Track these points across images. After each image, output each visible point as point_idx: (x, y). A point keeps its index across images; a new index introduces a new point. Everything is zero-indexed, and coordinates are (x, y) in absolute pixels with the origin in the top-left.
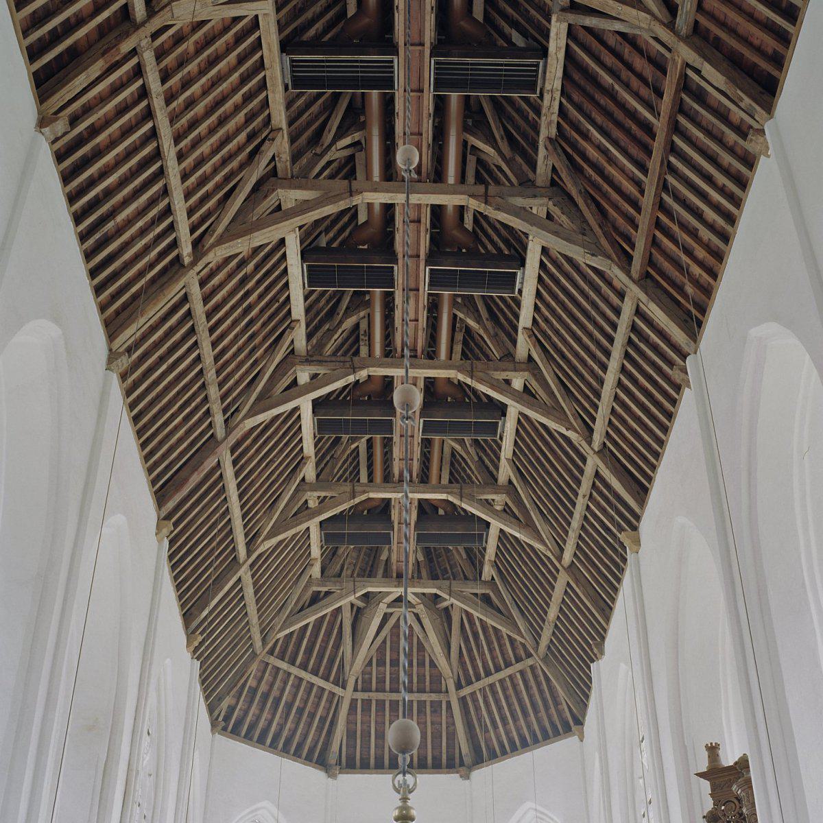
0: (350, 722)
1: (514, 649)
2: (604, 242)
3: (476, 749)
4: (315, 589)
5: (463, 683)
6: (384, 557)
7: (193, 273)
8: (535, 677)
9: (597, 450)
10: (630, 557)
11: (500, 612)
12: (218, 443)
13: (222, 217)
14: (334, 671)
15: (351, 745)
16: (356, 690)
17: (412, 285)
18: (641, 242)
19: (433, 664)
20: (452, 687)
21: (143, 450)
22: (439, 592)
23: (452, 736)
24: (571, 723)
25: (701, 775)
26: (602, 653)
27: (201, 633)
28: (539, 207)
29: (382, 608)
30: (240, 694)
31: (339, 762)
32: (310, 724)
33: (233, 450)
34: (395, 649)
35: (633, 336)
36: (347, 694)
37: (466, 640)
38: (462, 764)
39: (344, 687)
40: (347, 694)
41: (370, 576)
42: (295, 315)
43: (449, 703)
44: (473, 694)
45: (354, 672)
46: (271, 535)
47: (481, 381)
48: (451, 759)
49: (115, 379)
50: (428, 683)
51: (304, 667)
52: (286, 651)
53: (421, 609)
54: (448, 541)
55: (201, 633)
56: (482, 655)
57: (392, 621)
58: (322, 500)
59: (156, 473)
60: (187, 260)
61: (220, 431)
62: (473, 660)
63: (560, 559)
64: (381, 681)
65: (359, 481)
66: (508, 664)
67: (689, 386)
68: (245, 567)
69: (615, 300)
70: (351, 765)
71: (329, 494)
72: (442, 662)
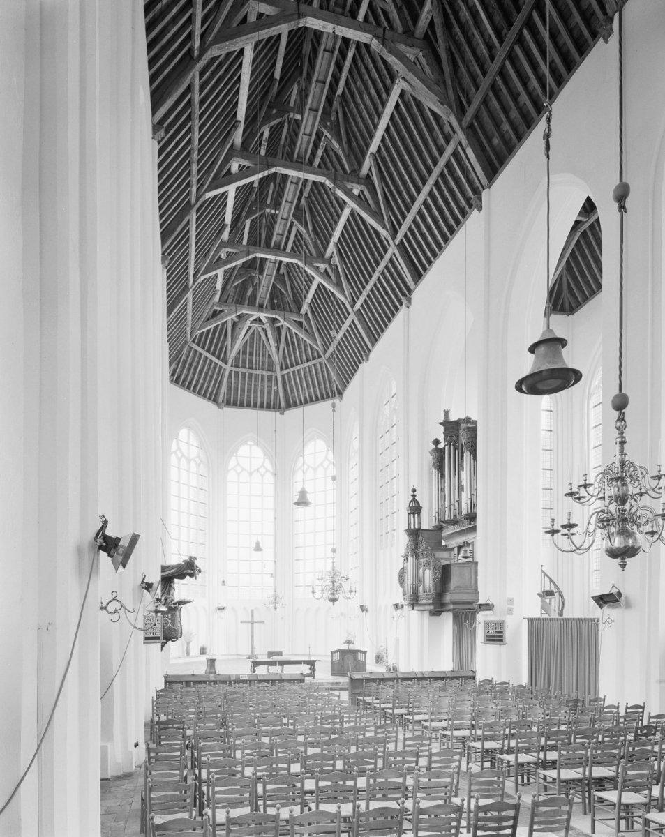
0: (229, 382)
1: (312, 353)
2: (451, 94)
3: (287, 401)
4: (215, 308)
5: (284, 368)
9: (397, 244)
11: (306, 331)
13: (218, 17)
14: (222, 354)
16: (232, 366)
17: (314, 107)
18: (477, 100)
19: (269, 356)
20: (278, 368)
22: (277, 317)
24: (336, 393)
25: (440, 423)
26: (368, 359)
28: (411, 53)
29: (248, 323)
30: (179, 362)
37: (288, 345)
38: (280, 407)
39: (226, 363)
40: (228, 368)
41: (240, 304)
43: (276, 377)
44: (288, 374)
45: (232, 356)
50: (266, 366)
52: (200, 341)
53: (267, 326)
56: (295, 354)
57: (251, 331)
62: (290, 356)
64: (244, 362)
66: (308, 360)
67: (480, 209)
69: (442, 140)
72: (274, 356)
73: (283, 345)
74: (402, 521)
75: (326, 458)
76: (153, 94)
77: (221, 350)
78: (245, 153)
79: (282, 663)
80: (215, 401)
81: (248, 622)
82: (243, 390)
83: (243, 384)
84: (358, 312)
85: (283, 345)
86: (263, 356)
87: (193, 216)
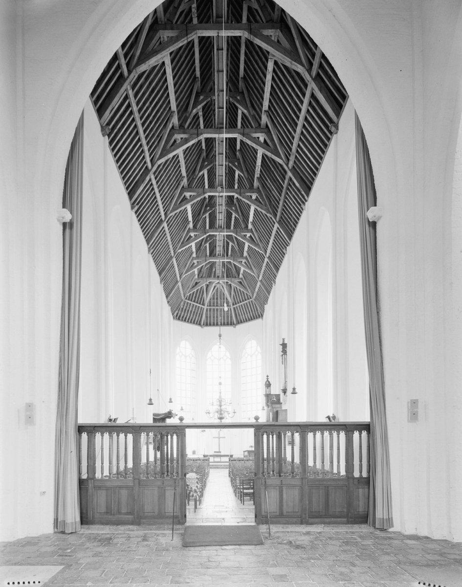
0: (206, 314)
6: (214, 270)
7: (165, 222)
8: (252, 304)
10: (273, 286)
11: (243, 285)
12: (149, 171)
15: (207, 320)
17: (220, 51)
19: (227, 299)
20: (231, 305)
21: (124, 180)
23: (231, 317)
27: (138, 204)
29: (214, 285)
31: (204, 324)
32: (196, 315)
33: (154, 173)
34: (217, 295)
35: (303, 130)
36: (205, 307)
38: (234, 324)
40: (205, 307)
42: (189, 220)
45: (207, 302)
46: (186, 273)
47: (238, 236)
48: (231, 322)
49: (151, 256)
51: (194, 301)
54: (230, 272)
55: (138, 204)
58: (196, 236)
59: (138, 213)
60: (163, 219)
61: (173, 255)
63: (258, 278)
64: (214, 303)
65: (200, 128)
66: (246, 300)
68: (165, 222)
70: (207, 324)
71: (198, 234)
73: (233, 293)
74: (261, 391)
75: (257, 350)
76: (129, 194)
77: (201, 299)
78: (195, 230)
79: (221, 456)
80: (200, 324)
81: (217, 437)
82: (214, 317)
83: (214, 314)
84: (269, 258)
85: (233, 293)
86: (224, 299)
87: (174, 260)
